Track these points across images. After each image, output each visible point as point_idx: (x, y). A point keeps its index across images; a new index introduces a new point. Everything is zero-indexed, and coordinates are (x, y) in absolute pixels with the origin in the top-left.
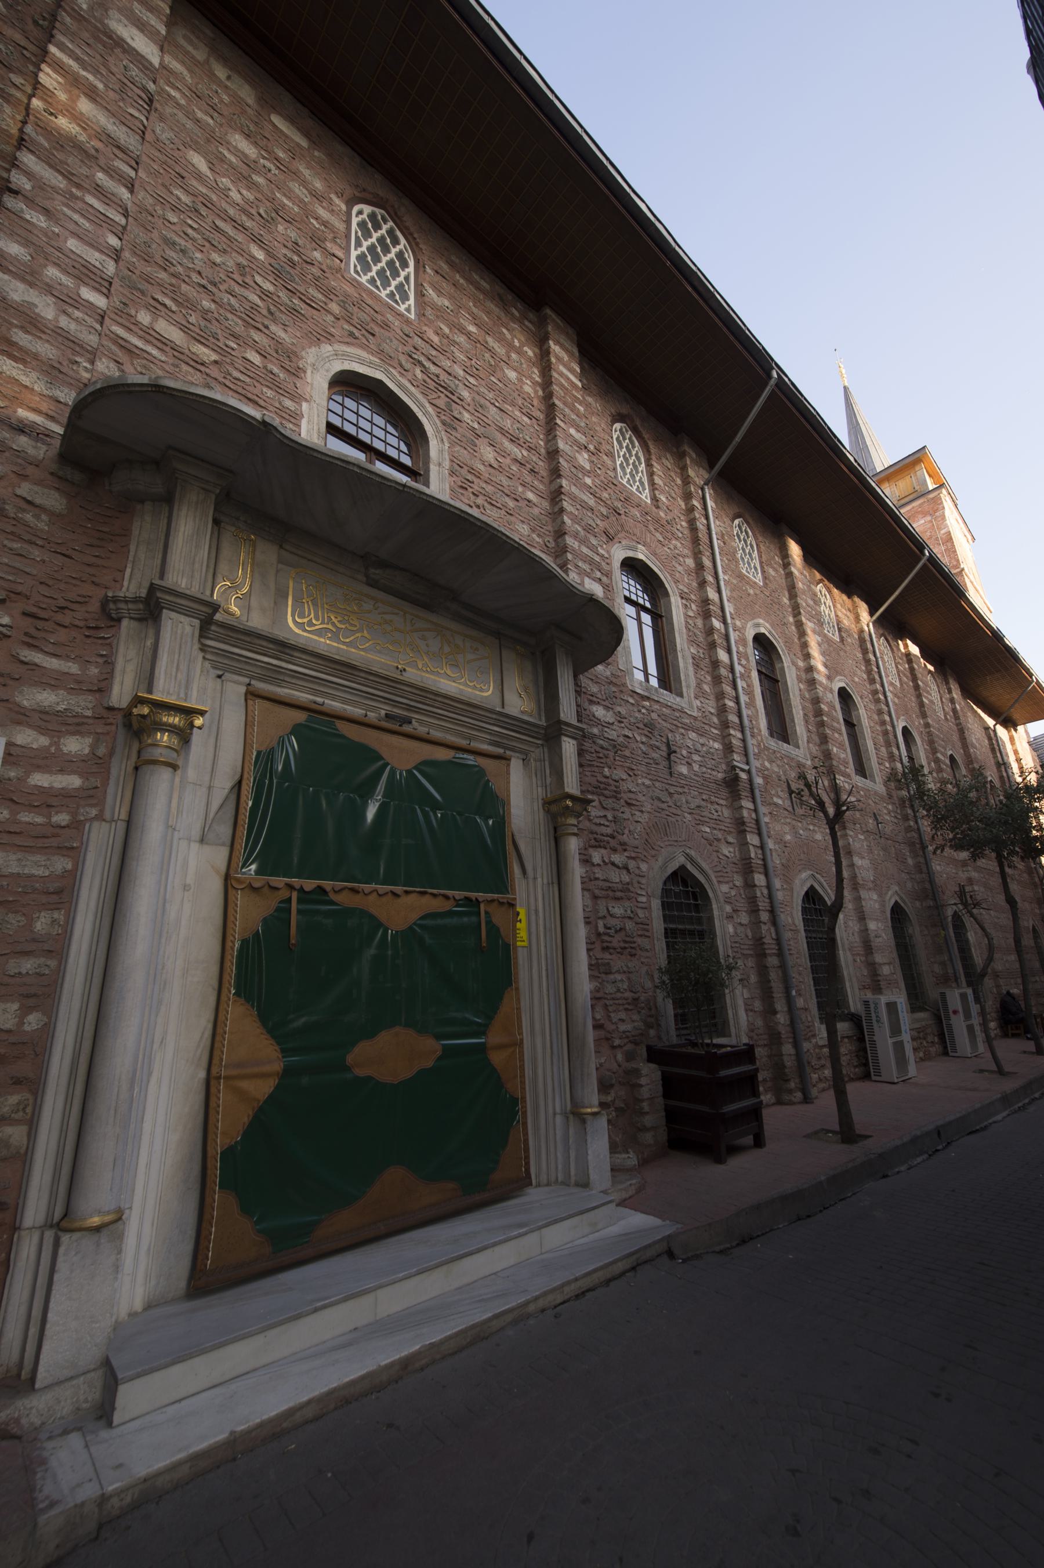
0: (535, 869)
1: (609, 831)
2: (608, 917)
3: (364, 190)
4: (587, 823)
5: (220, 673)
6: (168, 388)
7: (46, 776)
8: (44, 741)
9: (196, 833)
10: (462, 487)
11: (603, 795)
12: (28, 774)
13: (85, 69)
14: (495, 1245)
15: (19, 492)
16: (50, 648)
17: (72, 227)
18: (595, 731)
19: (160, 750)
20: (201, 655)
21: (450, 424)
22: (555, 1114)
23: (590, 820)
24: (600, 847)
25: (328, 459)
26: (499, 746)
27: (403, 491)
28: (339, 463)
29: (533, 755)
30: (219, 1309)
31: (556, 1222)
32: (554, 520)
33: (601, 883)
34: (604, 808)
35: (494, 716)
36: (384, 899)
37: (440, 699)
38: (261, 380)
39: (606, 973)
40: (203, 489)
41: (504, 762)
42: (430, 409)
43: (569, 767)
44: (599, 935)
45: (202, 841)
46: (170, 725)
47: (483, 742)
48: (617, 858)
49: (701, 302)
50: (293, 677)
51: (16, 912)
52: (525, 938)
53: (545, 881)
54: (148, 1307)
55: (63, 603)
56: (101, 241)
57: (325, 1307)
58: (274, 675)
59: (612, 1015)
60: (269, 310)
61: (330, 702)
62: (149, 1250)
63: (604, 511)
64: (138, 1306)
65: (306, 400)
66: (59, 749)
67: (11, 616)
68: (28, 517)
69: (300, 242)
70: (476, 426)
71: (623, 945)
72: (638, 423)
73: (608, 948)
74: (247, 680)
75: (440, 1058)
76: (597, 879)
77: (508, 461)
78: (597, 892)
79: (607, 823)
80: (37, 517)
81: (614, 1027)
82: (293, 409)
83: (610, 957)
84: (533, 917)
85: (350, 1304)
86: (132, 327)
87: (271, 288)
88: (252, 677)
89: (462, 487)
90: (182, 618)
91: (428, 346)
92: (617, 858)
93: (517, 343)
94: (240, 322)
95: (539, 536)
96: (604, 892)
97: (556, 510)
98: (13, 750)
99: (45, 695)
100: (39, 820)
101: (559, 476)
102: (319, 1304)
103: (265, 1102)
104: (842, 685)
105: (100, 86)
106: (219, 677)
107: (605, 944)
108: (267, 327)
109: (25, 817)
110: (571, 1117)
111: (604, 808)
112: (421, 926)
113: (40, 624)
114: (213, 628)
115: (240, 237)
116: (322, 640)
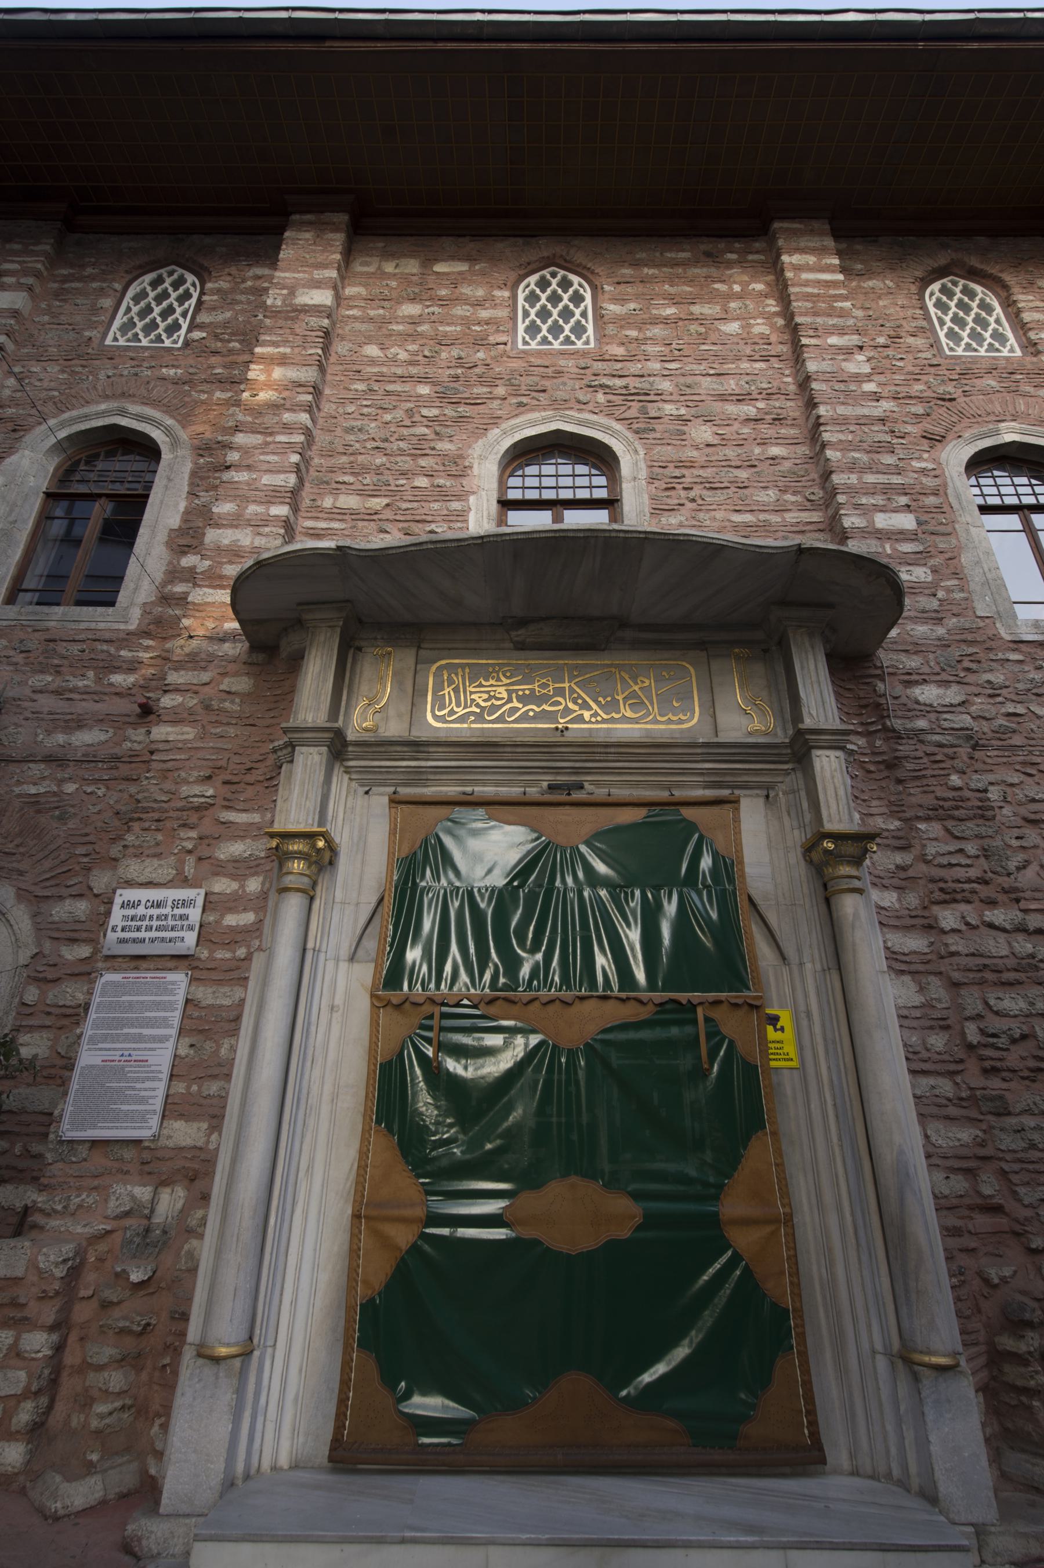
0: (799, 951)
1: (973, 873)
2: (990, 1016)
3: (529, 264)
4: (923, 868)
5: (367, 789)
6: (265, 560)
7: (235, 916)
8: (235, 885)
9: (345, 952)
10: (667, 489)
11: (953, 818)
12: (222, 916)
13: (278, 346)
14: (687, 1545)
15: (222, 687)
16: (241, 806)
17: (265, 467)
18: (922, 723)
19: (290, 877)
20: (346, 777)
21: (643, 428)
22: (874, 1352)
23: (927, 862)
24: (955, 901)
25: (402, 550)
26: (721, 787)
27: (483, 543)
28: (413, 548)
29: (783, 787)
30: (380, 1497)
31: (819, 1546)
32: (817, 463)
33: (964, 961)
34: (957, 838)
35: (699, 751)
36: (551, 1008)
37: (612, 750)
38: (429, 498)
39: (999, 1115)
40: (330, 627)
41: (727, 806)
42: (617, 426)
43: (831, 792)
44: (970, 1047)
45: (352, 959)
46: (296, 852)
47: (692, 787)
48: (998, 916)
49: (1004, 45)
50: (435, 773)
51: (211, 1039)
52: (792, 1055)
53: (818, 967)
54: (295, 1466)
55: (249, 765)
56: (287, 464)
57: (414, 1541)
58: (417, 777)
59: (1022, 1190)
60: (437, 434)
61: (481, 789)
62: (296, 1399)
63: (919, 409)
64: (284, 1461)
65: (473, 493)
66: (244, 891)
67: (215, 788)
68: (227, 704)
69: (463, 354)
70: (683, 411)
71: (1032, 1063)
72: (974, 262)
73: (995, 1070)
74: (392, 789)
75: (639, 1228)
76: (953, 954)
77: (736, 426)
78: (956, 976)
79: (964, 861)
80: (232, 702)
81: (1029, 1213)
82: (460, 508)
83: (1005, 1085)
84: (805, 1023)
85: (449, 1551)
86: (320, 515)
87: (435, 412)
88: (396, 785)
89: (667, 489)
90: (311, 749)
91: (613, 363)
92: (998, 916)
93: (737, 288)
94: (408, 458)
95: (795, 493)
96: (971, 975)
97: (818, 448)
98: (212, 898)
99: (237, 846)
100: (228, 955)
101: (815, 405)
102: (408, 1534)
103: (408, 1252)
105: (288, 350)
106: (367, 793)
107: (987, 1064)
108: (434, 449)
109: (220, 954)
110: (900, 1363)
111: (957, 838)
112: (602, 1041)
113: (234, 788)
114: (350, 749)
115: (407, 387)
116: (465, 726)
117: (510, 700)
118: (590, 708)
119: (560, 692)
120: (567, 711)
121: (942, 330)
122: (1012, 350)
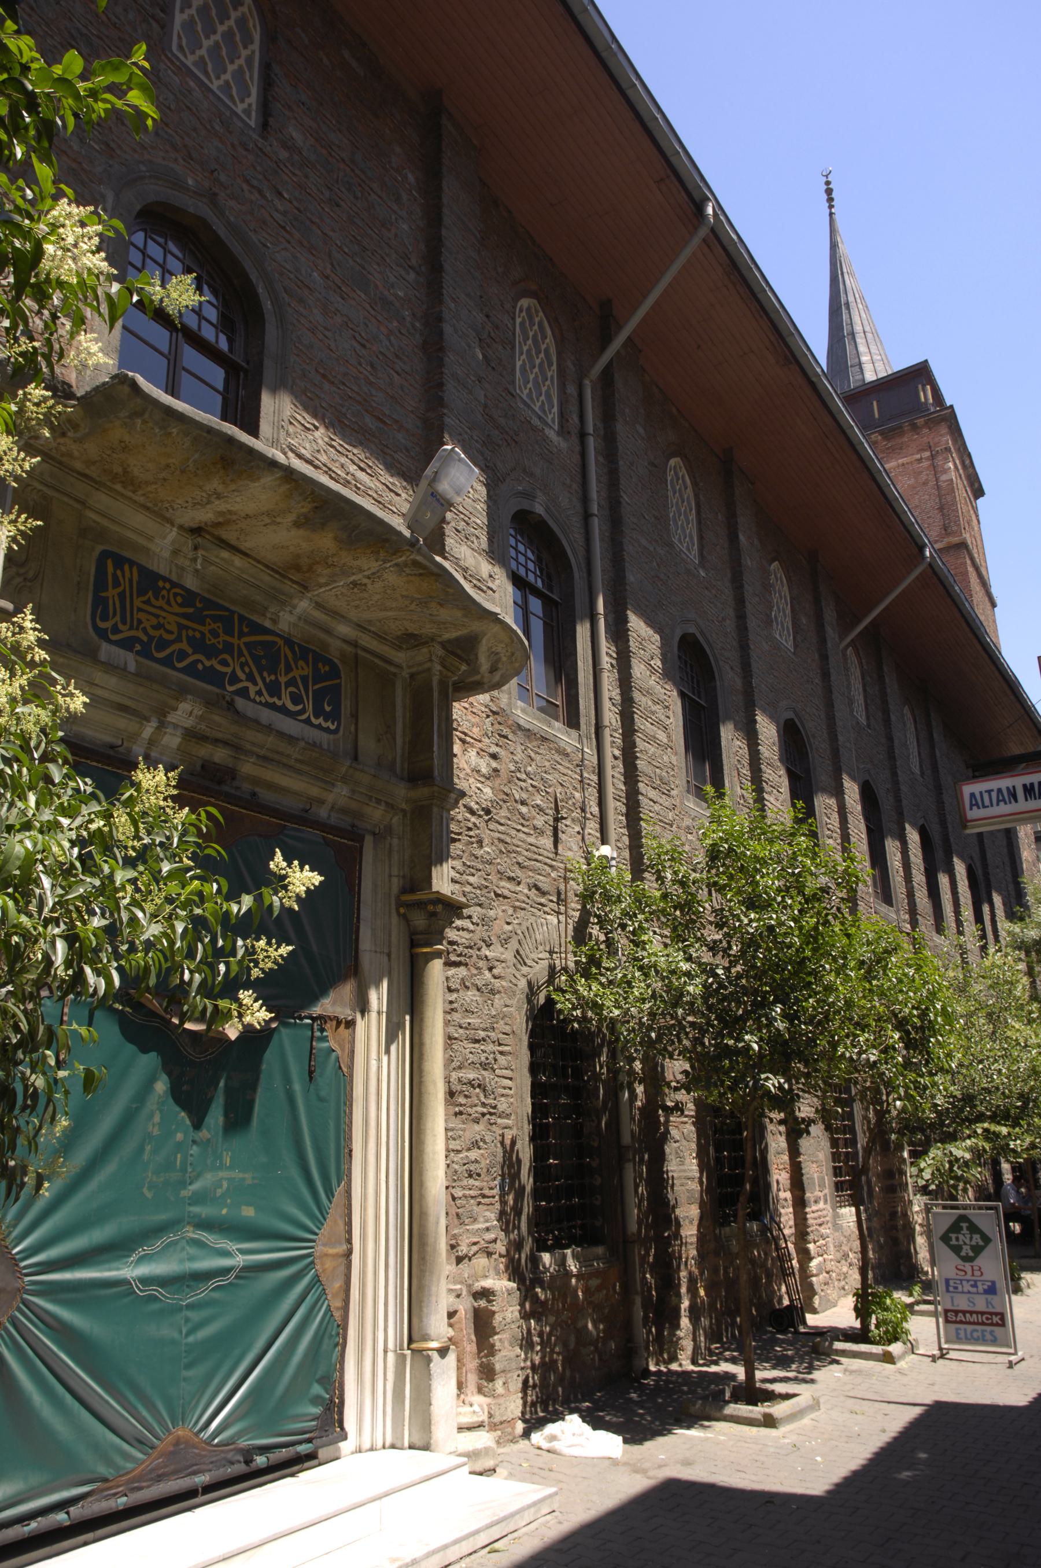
79: (472, 927)
104: (790, 715)
117: (179, 639)
118: (255, 684)
119: (228, 648)
120: (234, 679)
121: (182, 11)
122: (247, 112)
